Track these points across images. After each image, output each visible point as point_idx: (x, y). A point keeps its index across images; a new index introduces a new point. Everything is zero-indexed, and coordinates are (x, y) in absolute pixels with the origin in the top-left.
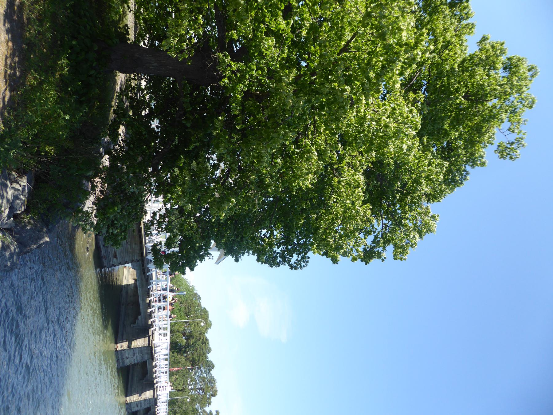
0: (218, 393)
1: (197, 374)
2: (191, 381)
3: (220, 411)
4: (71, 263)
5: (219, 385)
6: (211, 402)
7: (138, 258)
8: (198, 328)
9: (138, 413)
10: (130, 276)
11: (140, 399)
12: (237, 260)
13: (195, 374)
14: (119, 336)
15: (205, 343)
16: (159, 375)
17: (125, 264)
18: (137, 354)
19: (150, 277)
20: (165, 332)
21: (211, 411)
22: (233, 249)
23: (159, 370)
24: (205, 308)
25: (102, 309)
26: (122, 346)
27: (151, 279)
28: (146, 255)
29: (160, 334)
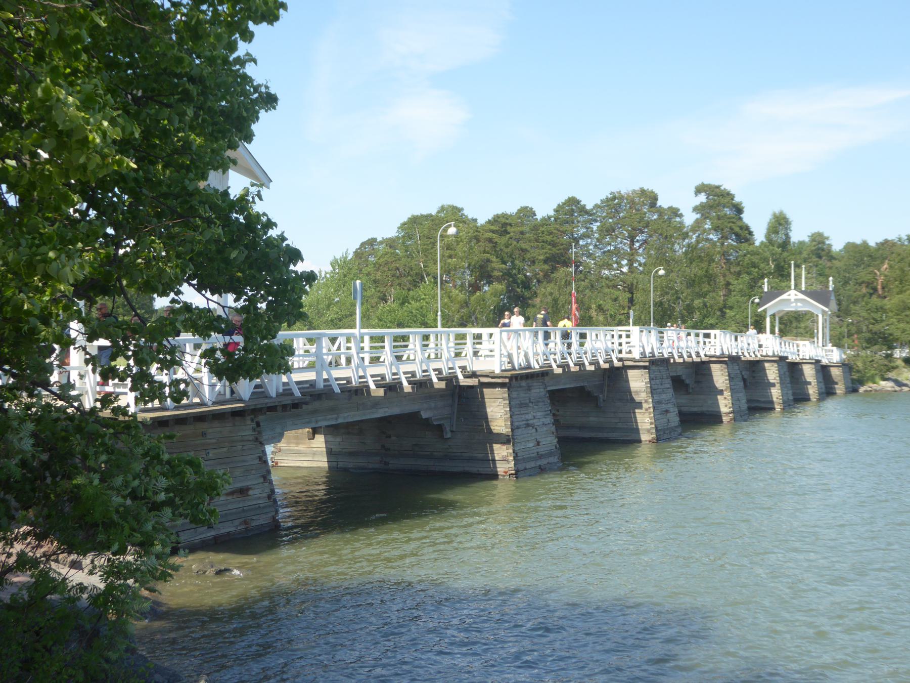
0: (648, 186)
1: (588, 246)
2: (609, 267)
3: (698, 182)
4: (254, 618)
5: (627, 185)
6: (670, 208)
7: (249, 424)
8: (461, 249)
9: (685, 409)
10: (302, 448)
11: (648, 405)
12: (270, 101)
13: (590, 256)
14: (474, 470)
15: (505, 225)
16: (589, 355)
17: (266, 462)
18: (530, 416)
19: (308, 388)
20: (469, 341)
21: (696, 209)
22: (234, 110)
23: (574, 356)
24: (403, 226)
25: (383, 521)
26: (505, 460)
27: (312, 384)
28: (241, 400)
29: (476, 354)
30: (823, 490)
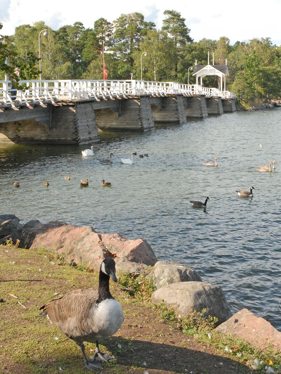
30: (104, 228)
